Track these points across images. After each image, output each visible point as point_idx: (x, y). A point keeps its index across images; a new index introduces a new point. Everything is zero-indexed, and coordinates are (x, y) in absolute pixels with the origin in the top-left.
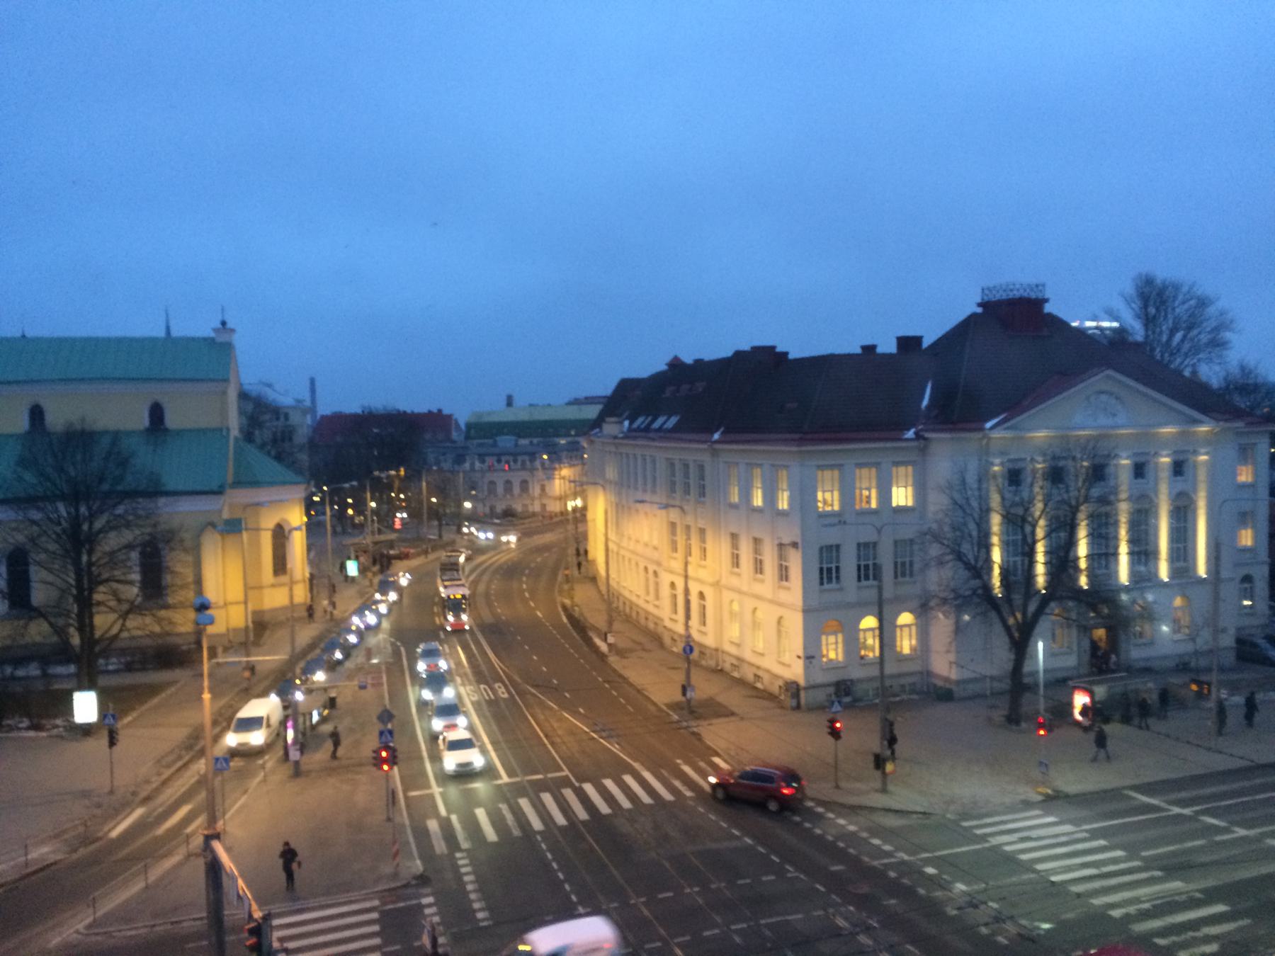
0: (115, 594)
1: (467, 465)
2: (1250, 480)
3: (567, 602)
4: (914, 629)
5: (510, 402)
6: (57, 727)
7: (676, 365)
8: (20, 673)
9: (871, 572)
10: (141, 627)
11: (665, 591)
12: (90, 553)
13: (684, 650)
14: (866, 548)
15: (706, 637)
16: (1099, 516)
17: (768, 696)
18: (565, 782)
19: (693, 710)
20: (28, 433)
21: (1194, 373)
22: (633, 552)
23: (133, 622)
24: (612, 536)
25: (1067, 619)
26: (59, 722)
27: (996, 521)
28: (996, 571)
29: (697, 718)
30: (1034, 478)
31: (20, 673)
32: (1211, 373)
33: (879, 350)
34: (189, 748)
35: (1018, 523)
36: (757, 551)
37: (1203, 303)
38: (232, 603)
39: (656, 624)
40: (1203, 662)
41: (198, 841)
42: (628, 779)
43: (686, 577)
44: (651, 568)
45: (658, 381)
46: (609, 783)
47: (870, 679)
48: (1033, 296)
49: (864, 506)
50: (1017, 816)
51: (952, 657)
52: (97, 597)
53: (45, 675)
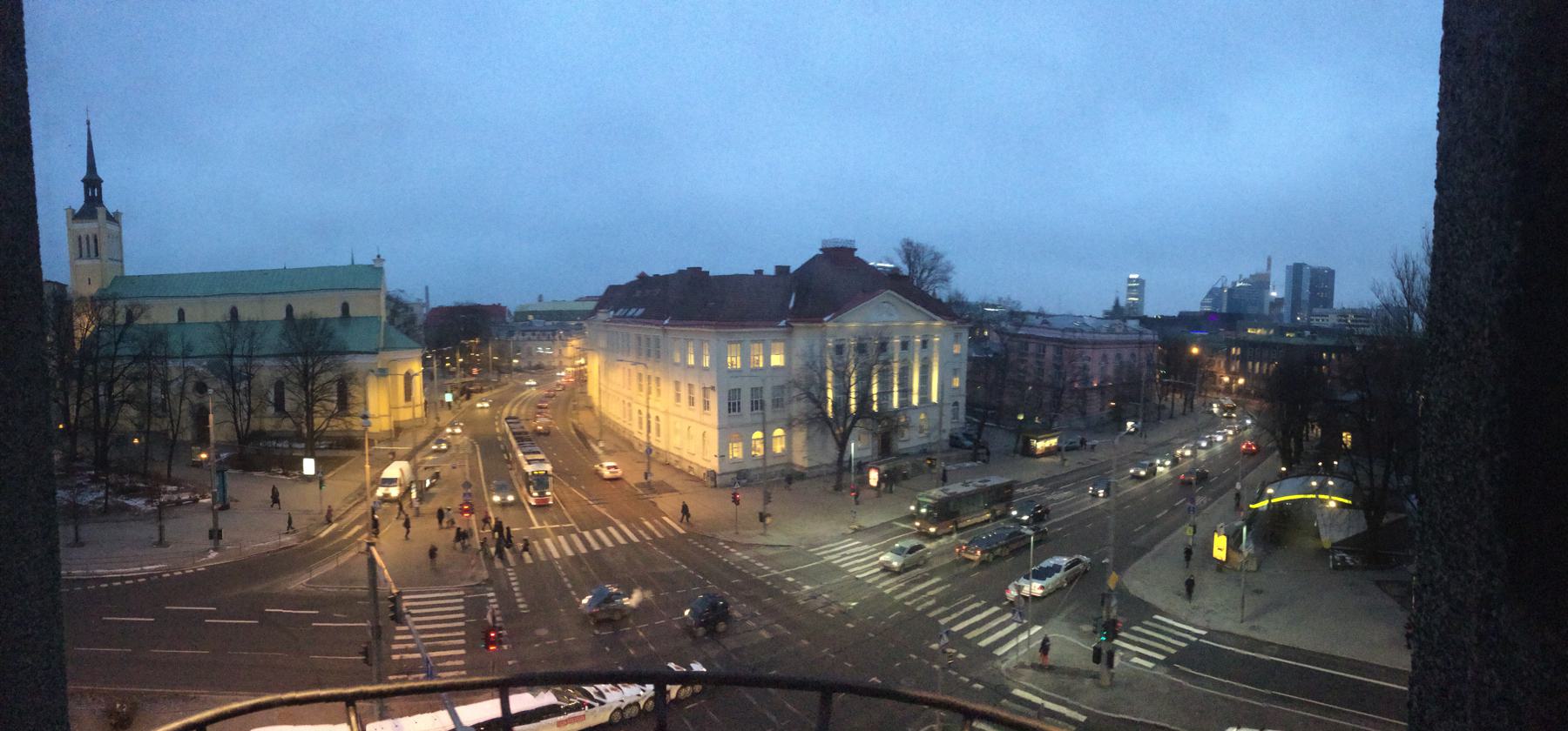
0: (323, 407)
1: (515, 338)
2: (959, 352)
3: (575, 421)
4: (784, 438)
5: (540, 299)
6: (295, 475)
7: (642, 277)
8: (279, 445)
9: (759, 405)
10: (337, 425)
12: (313, 385)
13: (646, 451)
14: (754, 390)
15: (659, 443)
16: (884, 371)
17: (696, 479)
18: (573, 530)
19: (650, 487)
20: (286, 319)
21: (934, 294)
23: (333, 423)
24: (602, 381)
25: (867, 429)
26: (297, 473)
27: (830, 374)
28: (830, 403)
29: (655, 492)
30: (850, 350)
31: (279, 445)
32: (943, 294)
33: (765, 273)
34: (360, 495)
35: (841, 375)
36: (690, 392)
37: (937, 257)
39: (630, 435)
40: (933, 448)
41: (364, 547)
42: (611, 529)
43: (648, 407)
44: (627, 401)
45: (631, 286)
46: (599, 532)
47: (758, 469)
48: (849, 246)
49: (756, 366)
50: (837, 544)
51: (805, 454)
52: (316, 408)
53: (290, 447)
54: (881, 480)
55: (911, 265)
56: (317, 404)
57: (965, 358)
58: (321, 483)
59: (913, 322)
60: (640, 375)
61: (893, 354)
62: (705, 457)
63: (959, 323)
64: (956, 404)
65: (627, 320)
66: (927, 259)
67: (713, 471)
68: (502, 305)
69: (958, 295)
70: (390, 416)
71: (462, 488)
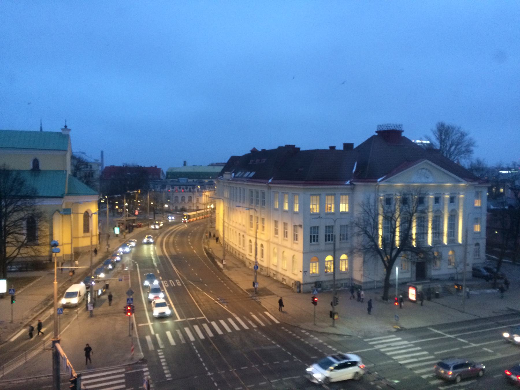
3: (207, 247)
4: (347, 261)
5: (185, 164)
10: (27, 252)
11: (247, 243)
12: (6, 221)
13: (255, 268)
15: (263, 263)
16: (421, 217)
17: (287, 287)
18: (204, 321)
21: (458, 162)
22: (234, 227)
23: (23, 251)
24: (226, 220)
27: (381, 219)
28: (380, 239)
32: (465, 163)
33: (337, 148)
35: (389, 219)
36: (285, 228)
37: (463, 135)
38: (65, 244)
42: (230, 320)
43: (256, 238)
44: (242, 234)
46: (222, 322)
47: (329, 281)
48: (398, 129)
49: (329, 211)
51: (362, 273)
52: (8, 240)
54: (418, 295)
55: (442, 141)
56: (10, 236)
57: (485, 210)
58: (13, 299)
59: (442, 183)
60: (251, 216)
61: (428, 207)
62: (293, 272)
63: (480, 183)
64: (477, 244)
65: (244, 179)
66: (455, 137)
67: (299, 282)
68: (158, 167)
69: (479, 162)
70: (71, 244)
71: (125, 294)
